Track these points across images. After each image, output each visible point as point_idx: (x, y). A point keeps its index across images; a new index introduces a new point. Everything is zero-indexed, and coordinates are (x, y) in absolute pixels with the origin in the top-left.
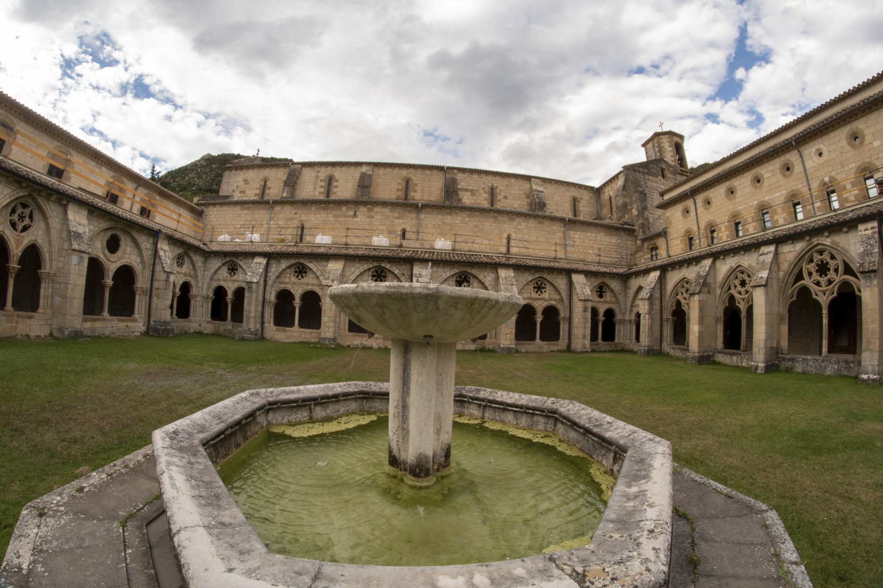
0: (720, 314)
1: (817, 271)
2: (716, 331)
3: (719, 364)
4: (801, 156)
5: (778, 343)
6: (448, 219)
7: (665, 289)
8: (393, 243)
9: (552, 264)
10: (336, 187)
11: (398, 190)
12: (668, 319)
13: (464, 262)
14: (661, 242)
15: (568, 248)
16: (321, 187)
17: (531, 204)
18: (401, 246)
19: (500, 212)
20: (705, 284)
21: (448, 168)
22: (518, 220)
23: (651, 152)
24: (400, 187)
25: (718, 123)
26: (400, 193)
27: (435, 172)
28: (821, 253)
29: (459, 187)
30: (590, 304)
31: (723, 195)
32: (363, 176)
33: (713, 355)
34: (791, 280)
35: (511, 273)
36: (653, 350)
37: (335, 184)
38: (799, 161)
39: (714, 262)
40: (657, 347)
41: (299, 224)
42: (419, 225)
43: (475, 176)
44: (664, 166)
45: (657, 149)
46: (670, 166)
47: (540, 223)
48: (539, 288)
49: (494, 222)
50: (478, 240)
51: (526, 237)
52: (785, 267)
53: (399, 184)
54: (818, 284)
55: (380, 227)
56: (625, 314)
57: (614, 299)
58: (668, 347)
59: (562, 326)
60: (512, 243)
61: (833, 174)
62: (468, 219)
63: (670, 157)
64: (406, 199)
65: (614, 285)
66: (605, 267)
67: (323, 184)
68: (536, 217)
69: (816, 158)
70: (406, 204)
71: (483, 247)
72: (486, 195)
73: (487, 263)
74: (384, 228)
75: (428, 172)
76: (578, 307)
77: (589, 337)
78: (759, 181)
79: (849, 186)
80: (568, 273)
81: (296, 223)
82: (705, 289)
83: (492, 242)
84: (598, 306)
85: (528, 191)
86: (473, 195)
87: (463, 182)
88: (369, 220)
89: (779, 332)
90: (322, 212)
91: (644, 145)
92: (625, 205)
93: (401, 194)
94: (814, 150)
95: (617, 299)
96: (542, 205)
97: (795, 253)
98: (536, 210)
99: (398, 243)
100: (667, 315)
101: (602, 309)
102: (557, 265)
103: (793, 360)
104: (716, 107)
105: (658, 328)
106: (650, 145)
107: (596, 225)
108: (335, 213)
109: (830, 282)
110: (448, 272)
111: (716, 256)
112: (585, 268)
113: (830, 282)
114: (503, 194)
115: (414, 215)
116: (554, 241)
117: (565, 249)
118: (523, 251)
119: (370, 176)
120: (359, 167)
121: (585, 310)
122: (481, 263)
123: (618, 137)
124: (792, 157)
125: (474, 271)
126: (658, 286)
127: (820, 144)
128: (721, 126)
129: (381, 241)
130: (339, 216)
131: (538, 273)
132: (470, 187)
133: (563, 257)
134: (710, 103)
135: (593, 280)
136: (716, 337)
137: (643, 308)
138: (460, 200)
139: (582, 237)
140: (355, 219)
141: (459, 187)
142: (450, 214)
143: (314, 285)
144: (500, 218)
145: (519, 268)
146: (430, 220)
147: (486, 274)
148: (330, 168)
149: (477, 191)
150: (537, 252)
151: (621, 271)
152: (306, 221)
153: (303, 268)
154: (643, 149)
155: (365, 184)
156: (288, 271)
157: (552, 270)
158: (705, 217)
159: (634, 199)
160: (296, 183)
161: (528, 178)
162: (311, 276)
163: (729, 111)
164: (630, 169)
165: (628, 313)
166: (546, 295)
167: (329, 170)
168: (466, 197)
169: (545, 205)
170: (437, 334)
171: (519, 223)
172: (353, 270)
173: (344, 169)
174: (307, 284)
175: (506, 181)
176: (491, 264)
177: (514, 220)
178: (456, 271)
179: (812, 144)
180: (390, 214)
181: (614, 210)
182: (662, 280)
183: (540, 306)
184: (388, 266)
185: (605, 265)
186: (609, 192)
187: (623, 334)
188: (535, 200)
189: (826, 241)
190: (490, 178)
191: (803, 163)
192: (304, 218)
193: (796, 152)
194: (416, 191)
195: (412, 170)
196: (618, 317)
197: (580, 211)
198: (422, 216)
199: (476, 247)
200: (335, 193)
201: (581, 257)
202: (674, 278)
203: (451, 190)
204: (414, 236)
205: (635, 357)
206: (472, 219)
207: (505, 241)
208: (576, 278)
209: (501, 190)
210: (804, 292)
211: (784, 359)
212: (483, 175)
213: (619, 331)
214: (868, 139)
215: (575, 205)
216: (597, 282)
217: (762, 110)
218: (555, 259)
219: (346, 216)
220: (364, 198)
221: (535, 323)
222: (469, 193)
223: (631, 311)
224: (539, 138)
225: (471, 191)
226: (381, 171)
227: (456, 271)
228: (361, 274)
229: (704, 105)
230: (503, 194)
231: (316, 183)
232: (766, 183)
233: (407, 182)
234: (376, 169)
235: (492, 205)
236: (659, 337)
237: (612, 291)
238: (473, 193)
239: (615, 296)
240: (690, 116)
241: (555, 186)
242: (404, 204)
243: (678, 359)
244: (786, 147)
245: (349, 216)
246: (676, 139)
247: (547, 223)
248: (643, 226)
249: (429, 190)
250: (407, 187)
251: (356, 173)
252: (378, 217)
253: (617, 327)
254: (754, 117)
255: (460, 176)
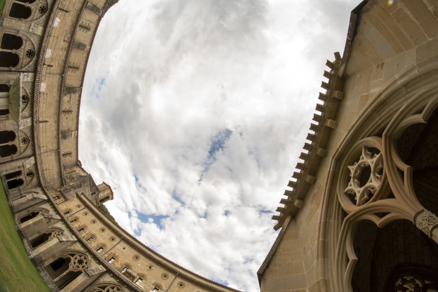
0: (42, 232)
1: (82, 264)
2: (35, 234)
3: (23, 242)
4: (119, 242)
5: (45, 260)
6: (55, 90)
7: (41, 205)
8: (47, 60)
9: (36, 146)
10: (83, 31)
11: (74, 63)
12: (29, 211)
13: (33, 99)
14: (62, 199)
15: (46, 153)
16: (86, 23)
17: (65, 132)
18: (44, 64)
19: (59, 116)
20: (50, 219)
21: (81, 89)
22: (56, 125)
23: (102, 187)
24: (75, 64)
25: (129, 217)
26: (72, 64)
27: (80, 82)
28: (85, 258)
29: (72, 94)
30: (22, 169)
31: (91, 219)
32: (85, 46)
33: (24, 237)
34: (70, 253)
35: (29, 124)
36: (13, 209)
37: (85, 31)
38: (118, 242)
39: (76, 241)
40: (15, 211)
41: (69, 10)
42: (54, 74)
43: (77, 103)
44: (96, 193)
45: (103, 189)
46: (98, 196)
47: (56, 137)
48: (24, 141)
49: (54, 113)
50: (45, 106)
51: (48, 131)
52: (72, 248)
53: (77, 64)
54: (75, 263)
55: (55, 54)
56: (24, 190)
57: (28, 182)
58: (17, 216)
59: (9, 157)
60: (44, 124)
61: (120, 256)
62: (55, 100)
63: (102, 195)
64: (69, 67)
65: (35, 180)
66: (42, 174)
67: (87, 25)
68: (58, 134)
69: (121, 248)
70: (66, 66)
71: (41, 109)
72: (68, 108)
73: (33, 111)
74: (55, 56)
75: (80, 79)
76: (19, 163)
77: (7, 173)
78: (103, 231)
79: (119, 263)
80: (34, 154)
81: (71, 8)
82: (48, 220)
83: (44, 113)
84: (23, 174)
85: (71, 130)
86: (68, 102)
87: (74, 97)
88: (61, 48)
89: (49, 259)
90: (71, 24)
91: (104, 183)
92: (73, 178)
93: (72, 65)
94: (124, 246)
95: (29, 184)
96: (65, 137)
97: (79, 249)
98: (62, 135)
99: (46, 63)
100: (31, 210)
101: (22, 177)
102: (37, 148)
103: (43, 270)
104: (134, 214)
105: (23, 208)
106: (104, 185)
107: (60, 166)
108: (69, 31)
109: (78, 267)
110: (29, 91)
111: (63, 220)
112: (38, 163)
113: (78, 267)
114: (68, 117)
115: (59, 72)
116: (48, 145)
117: (45, 152)
118: (41, 130)
119: (84, 49)
120: (89, 44)
121: (19, 167)
122: (33, 108)
123: (107, 174)
124: (118, 239)
125: (29, 105)
126: (41, 200)
127: (128, 247)
128: (128, 219)
129: (48, 54)
130: (66, 32)
131: (31, 139)
132: (72, 100)
133: (41, 152)
134: (135, 212)
135: (34, 168)
136: (32, 235)
137: (29, 197)
138: (65, 95)
139: (53, 160)
140: (62, 41)
141: (72, 94)
142: (58, 90)
143: (34, 16)
144: (56, 116)
145: (32, 128)
146: (56, 80)
147: (28, 111)
148: (94, 29)
149: (70, 104)
150: (42, 137)
151: (42, 182)
152: (69, 14)
153: (44, 12)
154: (102, 183)
155: (80, 46)
156: (45, 3)
157: (34, 145)
158: (79, 215)
159: (77, 182)
160: (93, 11)
161: (77, 129)
162: (39, 15)
163: (136, 221)
164: (90, 178)
165: (24, 192)
166: (22, 145)
167: (93, 29)
168: (67, 98)
169: (65, 139)
170: (11, 105)
171: (54, 126)
172: (36, 40)
173: (91, 37)
174: (35, 13)
175: (75, 118)
176: (33, 113)
177: (56, 123)
178: (29, 95)
179: (126, 244)
180: (61, 59)
181: (70, 174)
182: (44, 201)
183: (16, 142)
184: (34, 59)
185: (43, 174)
186: (77, 170)
187: (14, 192)
188: (66, 134)
189: (90, 258)
190: (76, 110)
191: (118, 244)
192: (71, 13)
193: (120, 240)
194: (72, 72)
195: (82, 71)
196: (21, 187)
197: (66, 157)
198: (58, 76)
199: (41, 104)
200: (80, 30)
201: (44, 161)
202: (47, 206)
203: (70, 90)
204: (48, 71)
205: (6, 202)
206: (55, 102)
207: (44, 119)
208: (33, 158)
209: (70, 116)
210: (69, 260)
211: (41, 266)
212: (77, 106)
213: (15, 190)
214: (138, 262)
215: (68, 154)
216: (34, 171)
217: (143, 233)
218: (39, 147)
219: (65, 36)
220: (73, 44)
221: (7, 142)
222: (69, 99)
223: (26, 193)
224: (100, 136)
225: (70, 101)
226: (85, 55)
227: (29, 95)
228: (33, 44)
229: (133, 210)
230: (68, 117)
231: (89, 21)
232: (103, 233)
233: (77, 68)
234: (87, 53)
235: (63, 112)
236: (20, 210)
237: (32, 180)
238: (69, 102)
239: (30, 182)
240: (126, 205)
241: (75, 143)
242: (65, 67)
243: (15, 223)
244: (120, 236)
245: (65, 37)
246: (111, 196)
247: (56, 140)
248: (67, 189)
249: (71, 79)
250: (74, 68)
251: (87, 43)
252: (61, 53)
253: (16, 188)
254: (139, 232)
255: (77, 95)
